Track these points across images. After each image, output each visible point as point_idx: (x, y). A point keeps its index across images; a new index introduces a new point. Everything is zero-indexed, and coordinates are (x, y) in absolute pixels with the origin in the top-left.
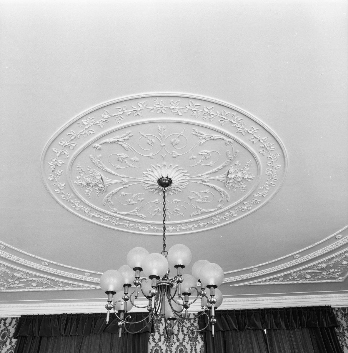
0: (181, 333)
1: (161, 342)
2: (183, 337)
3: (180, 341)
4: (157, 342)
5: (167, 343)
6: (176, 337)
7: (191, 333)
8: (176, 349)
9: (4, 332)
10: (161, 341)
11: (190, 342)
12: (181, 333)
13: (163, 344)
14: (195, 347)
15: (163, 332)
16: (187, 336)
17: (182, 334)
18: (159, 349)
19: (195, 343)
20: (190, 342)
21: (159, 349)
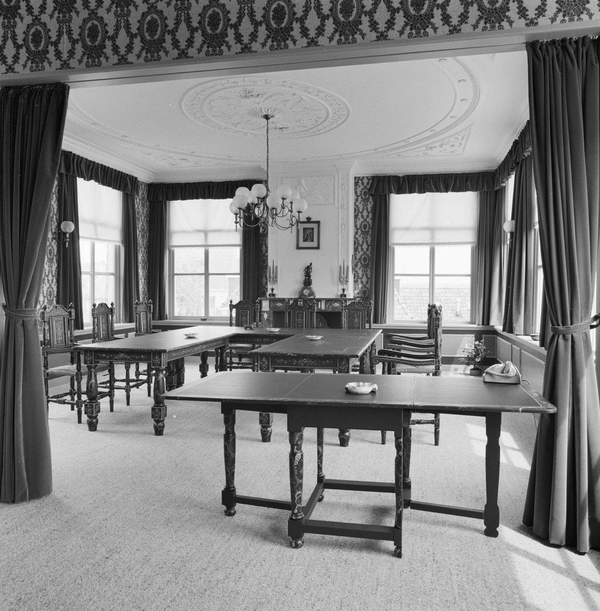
0: (183, 26)
1: (134, 54)
2: (318, 22)
3: (35, 14)
4: (11, 63)
5: (61, 15)
6: (300, 26)
7: (208, 25)
8: (80, 27)
9: (149, 18)
10: (75, 56)
11: (114, 8)
12: (183, 26)
13: (51, 16)
14: (67, 24)
15: (78, 33)
16: (80, 43)
17: (186, 29)
18: (42, 31)
19: (68, 15)
20: (56, 15)
21: (285, 6)
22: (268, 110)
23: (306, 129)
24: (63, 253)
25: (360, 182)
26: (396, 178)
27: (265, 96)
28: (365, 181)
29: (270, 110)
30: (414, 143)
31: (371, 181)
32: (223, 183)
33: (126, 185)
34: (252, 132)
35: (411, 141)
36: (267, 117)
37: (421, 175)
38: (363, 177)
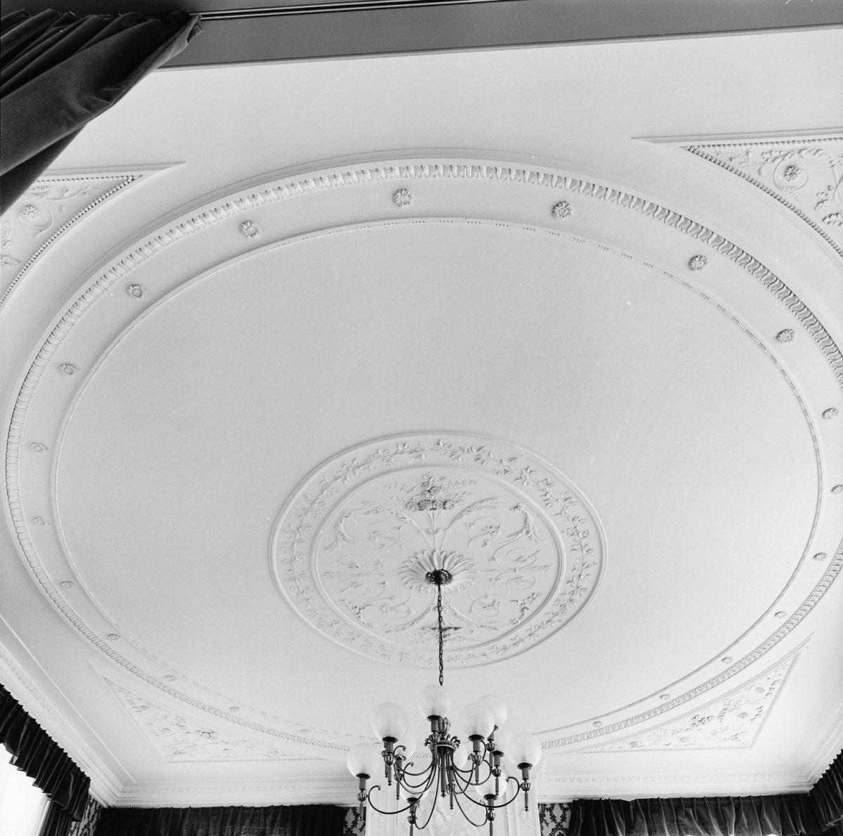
22: (445, 559)
23: (496, 634)
24: (26, 652)
25: (547, 814)
26: (620, 805)
27: (458, 508)
28: (558, 813)
29: (448, 560)
30: (613, 728)
31: (568, 814)
32: (265, 809)
33: (65, 786)
34: (171, 816)
35: (605, 722)
36: (437, 578)
37: (668, 800)
38: (553, 805)
